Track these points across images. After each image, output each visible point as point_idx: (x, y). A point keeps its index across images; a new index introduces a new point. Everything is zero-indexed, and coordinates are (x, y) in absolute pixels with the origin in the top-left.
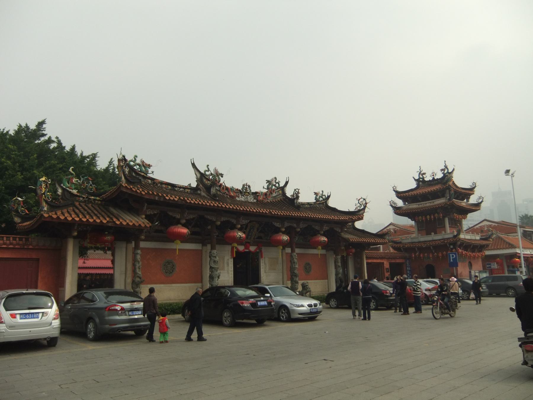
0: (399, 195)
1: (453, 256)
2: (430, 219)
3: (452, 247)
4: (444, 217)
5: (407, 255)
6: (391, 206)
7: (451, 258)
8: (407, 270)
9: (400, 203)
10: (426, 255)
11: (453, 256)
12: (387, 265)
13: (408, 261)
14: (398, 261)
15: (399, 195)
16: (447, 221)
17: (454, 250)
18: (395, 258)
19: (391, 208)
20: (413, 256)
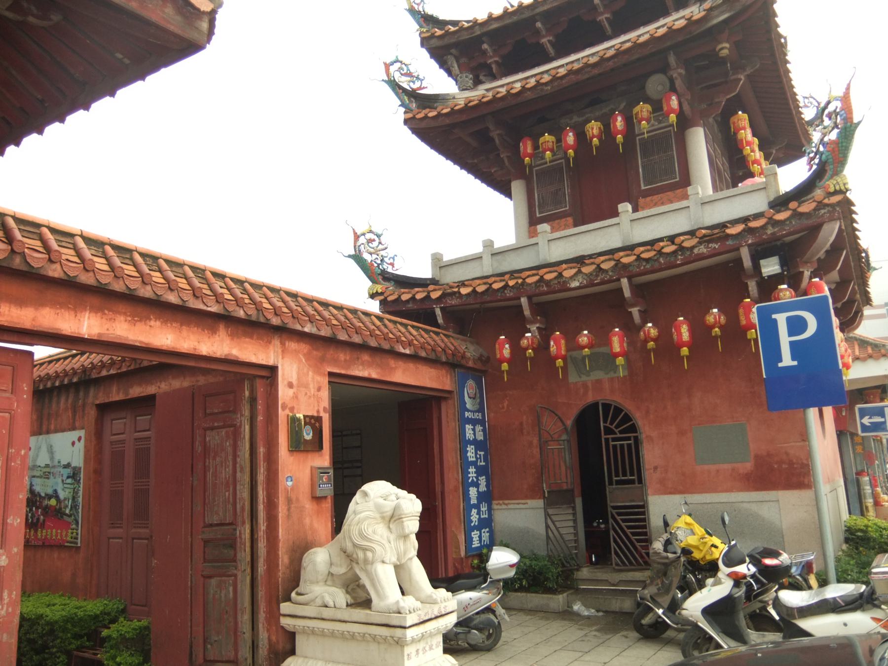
0: (451, 44)
1: (797, 325)
2: (607, 132)
3: (771, 267)
4: (685, 123)
5: (469, 350)
6: (394, 85)
7: (785, 340)
8: (464, 443)
9: (438, 82)
10: (584, 337)
11: (797, 325)
12: (302, 388)
13: (470, 387)
14: (404, 375)
15: (451, 44)
16: (699, 144)
17: (785, 291)
18: (383, 352)
19: (393, 100)
20: (507, 351)
